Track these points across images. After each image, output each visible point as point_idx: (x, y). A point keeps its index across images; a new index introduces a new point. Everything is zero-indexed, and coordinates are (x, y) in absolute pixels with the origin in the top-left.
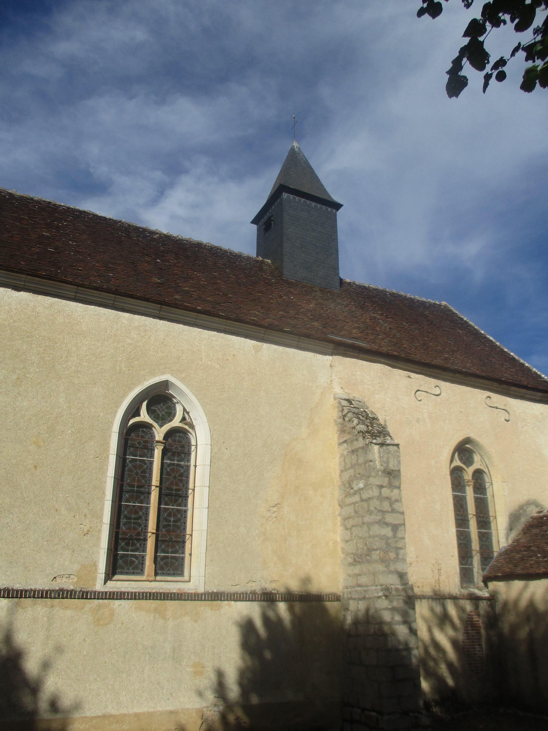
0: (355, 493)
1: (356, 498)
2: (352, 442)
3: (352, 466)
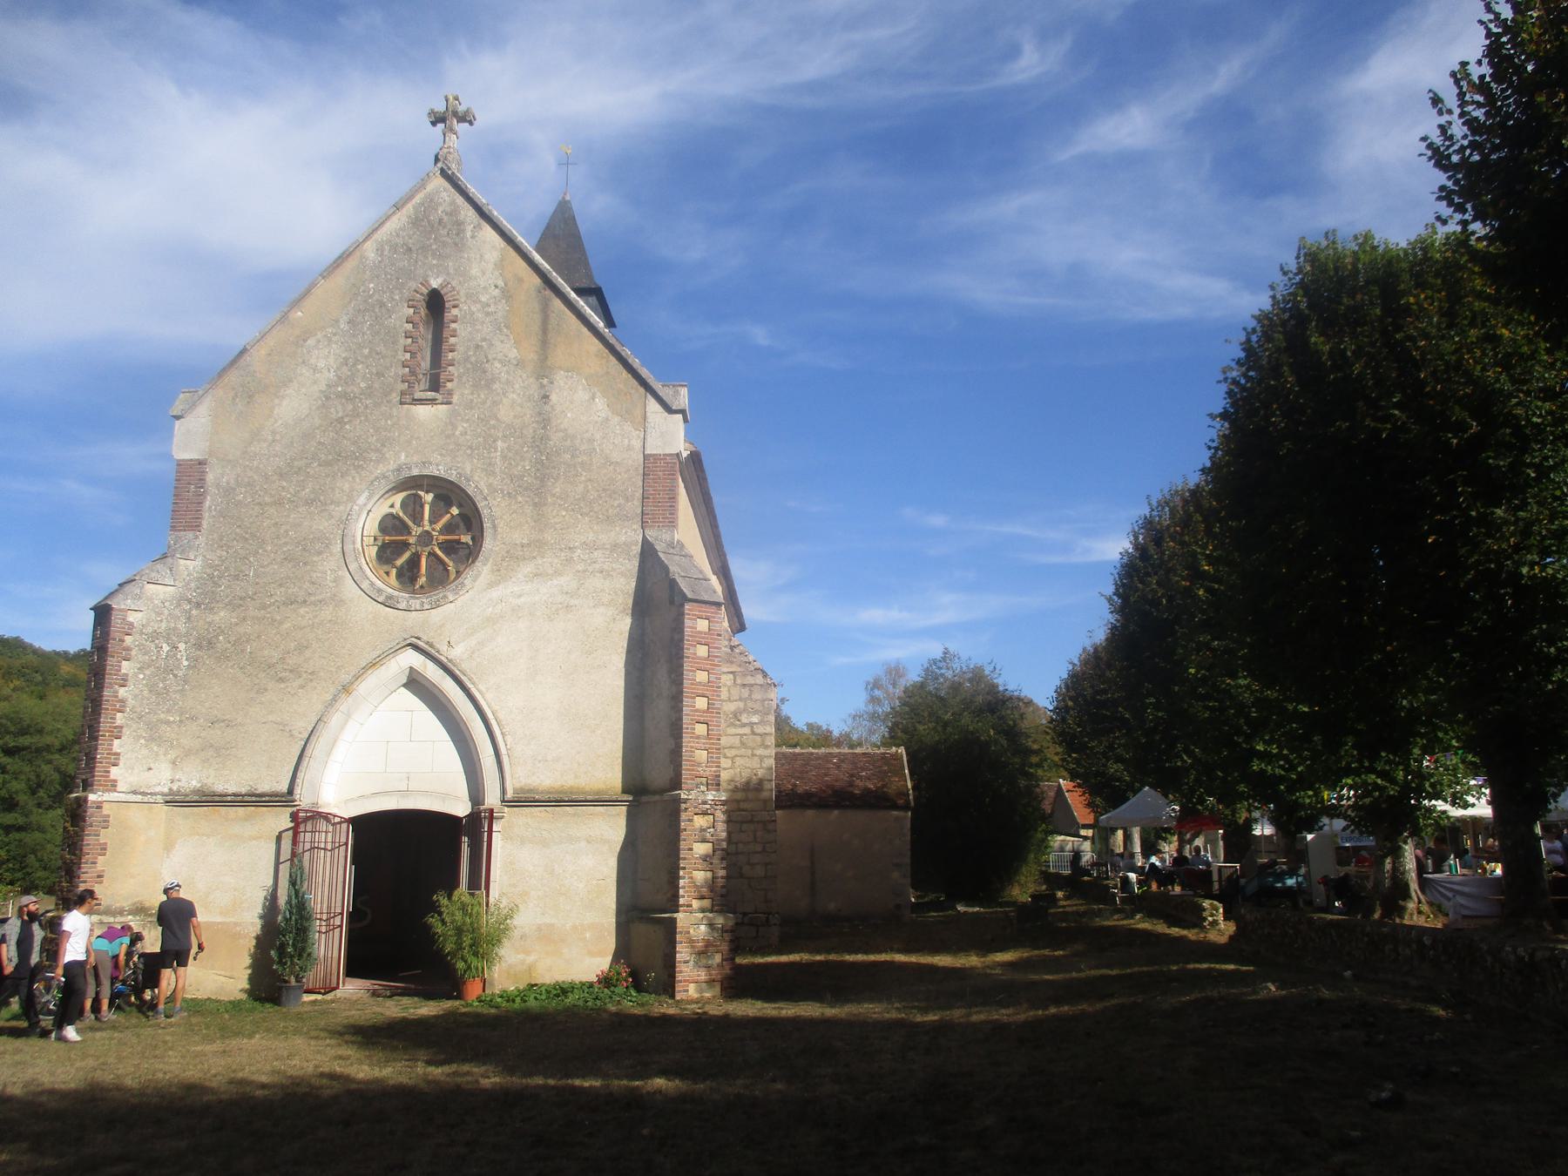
0: (744, 725)
1: (747, 730)
2: (745, 675)
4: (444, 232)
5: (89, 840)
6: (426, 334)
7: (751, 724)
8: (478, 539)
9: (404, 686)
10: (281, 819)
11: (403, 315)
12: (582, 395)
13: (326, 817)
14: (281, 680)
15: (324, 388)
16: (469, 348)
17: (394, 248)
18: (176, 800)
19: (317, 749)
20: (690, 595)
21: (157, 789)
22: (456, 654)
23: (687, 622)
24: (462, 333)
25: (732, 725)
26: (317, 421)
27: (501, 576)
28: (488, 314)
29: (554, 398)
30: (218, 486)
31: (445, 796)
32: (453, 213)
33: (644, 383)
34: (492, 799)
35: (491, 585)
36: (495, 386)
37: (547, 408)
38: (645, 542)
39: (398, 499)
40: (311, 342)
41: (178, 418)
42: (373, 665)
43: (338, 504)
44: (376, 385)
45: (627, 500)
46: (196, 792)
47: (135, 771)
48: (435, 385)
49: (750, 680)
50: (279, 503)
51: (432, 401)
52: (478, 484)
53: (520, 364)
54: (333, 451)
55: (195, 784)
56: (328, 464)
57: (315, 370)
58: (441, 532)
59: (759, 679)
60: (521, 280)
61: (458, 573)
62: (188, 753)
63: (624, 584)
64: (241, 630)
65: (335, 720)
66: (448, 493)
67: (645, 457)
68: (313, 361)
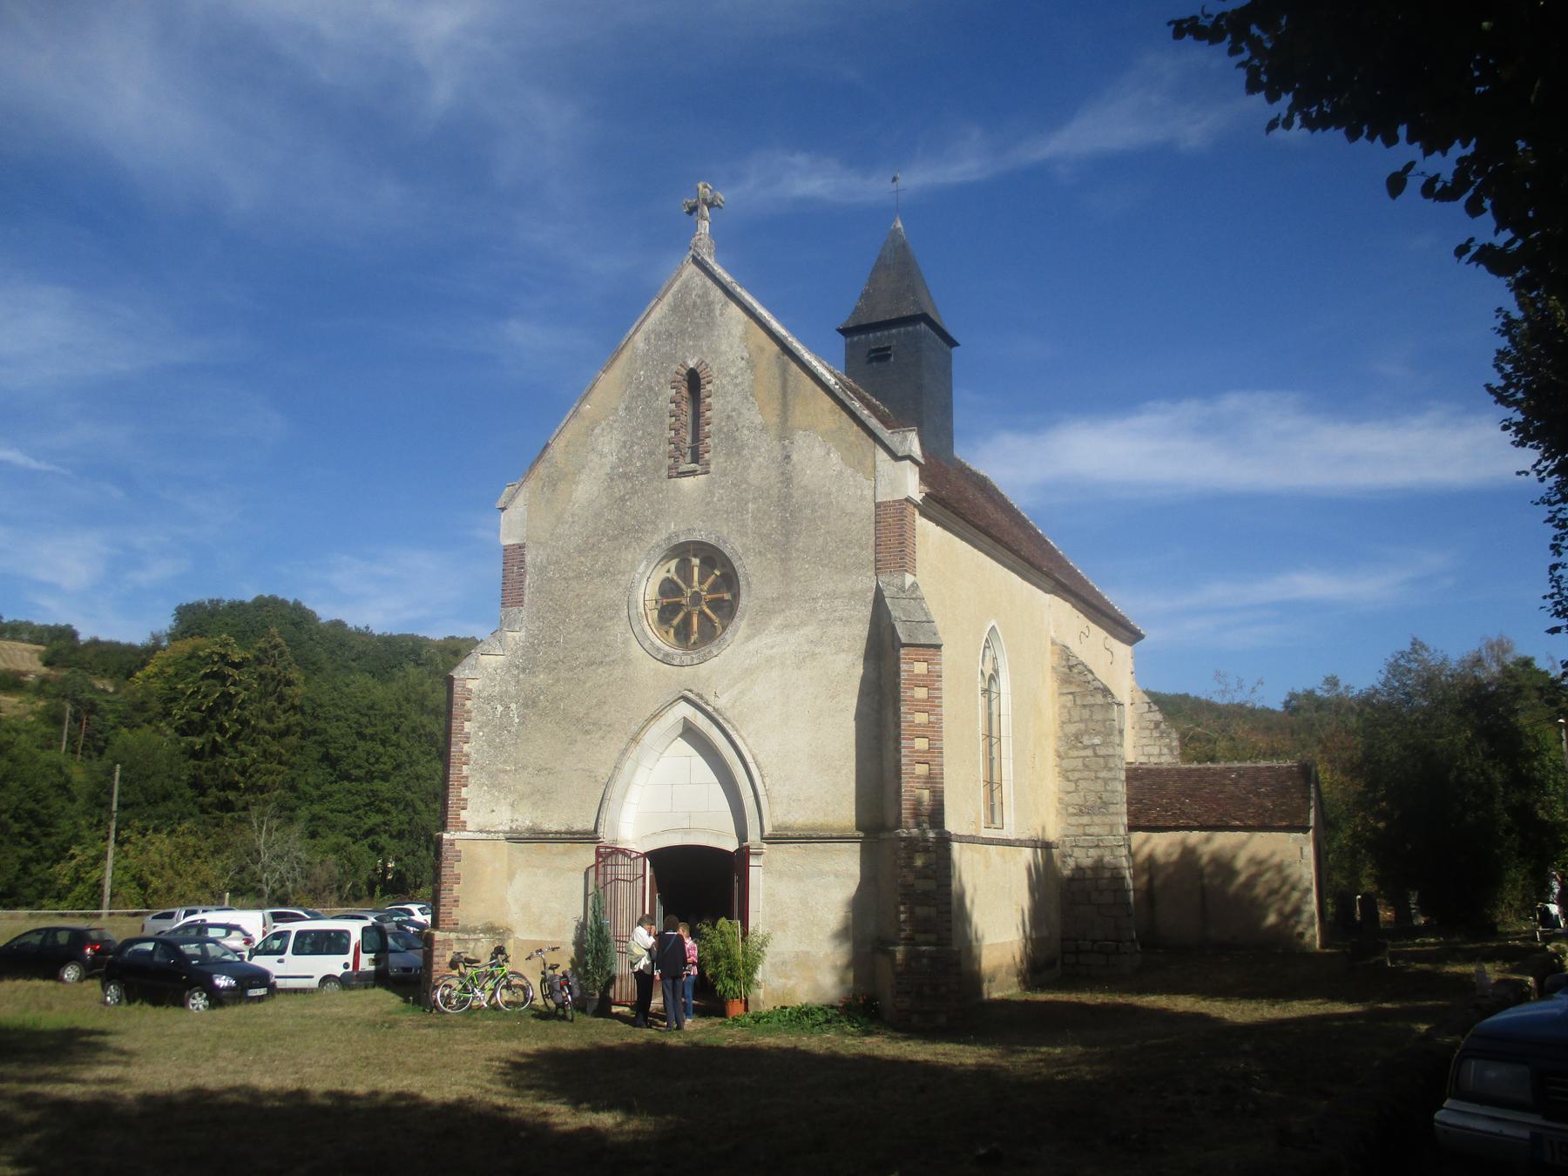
0: (1086, 747)
1: (1089, 752)
2: (1084, 696)
3: (1081, 721)
4: (697, 314)
5: (444, 871)
6: (687, 408)
7: (1094, 746)
8: (736, 596)
9: (681, 736)
10: (587, 855)
12: (819, 451)
13: (624, 852)
14: (587, 733)
17: (658, 335)
18: (515, 838)
20: (904, 640)
21: (500, 828)
22: (721, 702)
23: (903, 667)
24: (715, 406)
25: (1075, 747)
26: (605, 502)
27: (756, 629)
28: (736, 385)
29: (795, 457)
30: (534, 566)
31: (719, 834)
32: (705, 295)
33: (872, 434)
34: (753, 837)
35: (748, 638)
37: (789, 467)
39: (673, 564)
41: (503, 509)
42: (655, 716)
45: (862, 548)
46: (529, 830)
47: (481, 812)
48: (696, 458)
49: (1090, 700)
50: (579, 577)
51: (693, 473)
56: (615, 538)
57: (602, 455)
58: (709, 591)
59: (1099, 699)
60: (762, 350)
61: (724, 628)
62: (522, 797)
63: (858, 631)
65: (628, 765)
66: (712, 556)
67: (878, 506)
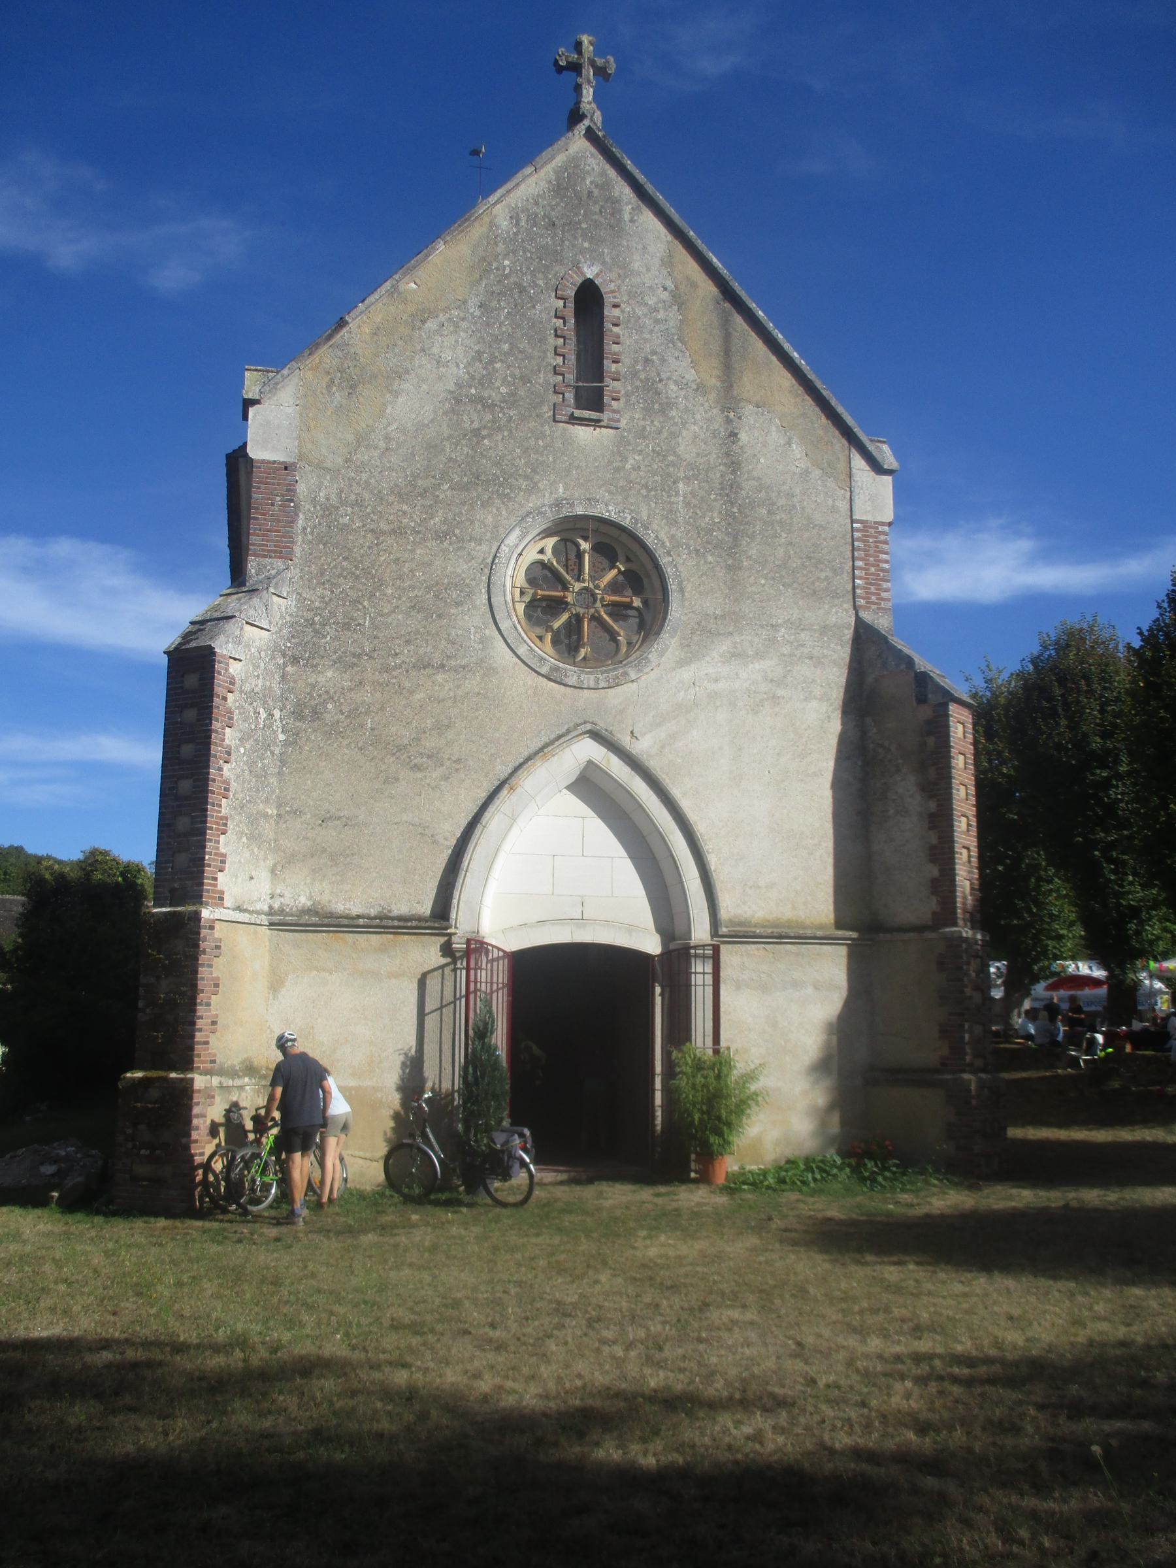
9: (568, 788)
11: (551, 309)
12: (775, 437)
14: (417, 768)
15: (452, 388)
16: (636, 362)
17: (533, 219)
19: (475, 858)
21: (259, 906)
24: (625, 343)
26: (446, 431)
28: (657, 321)
29: (743, 436)
30: (314, 502)
31: (631, 928)
32: (606, 186)
34: (700, 932)
35: (681, 663)
36: (673, 413)
37: (735, 448)
38: (859, 622)
40: (431, 325)
43: (480, 542)
44: (522, 393)
51: (596, 423)
52: (656, 535)
53: (701, 389)
54: (465, 472)
55: (304, 901)
60: (694, 285)
63: (830, 677)
64: (357, 697)
66: (616, 544)
68: (435, 350)
